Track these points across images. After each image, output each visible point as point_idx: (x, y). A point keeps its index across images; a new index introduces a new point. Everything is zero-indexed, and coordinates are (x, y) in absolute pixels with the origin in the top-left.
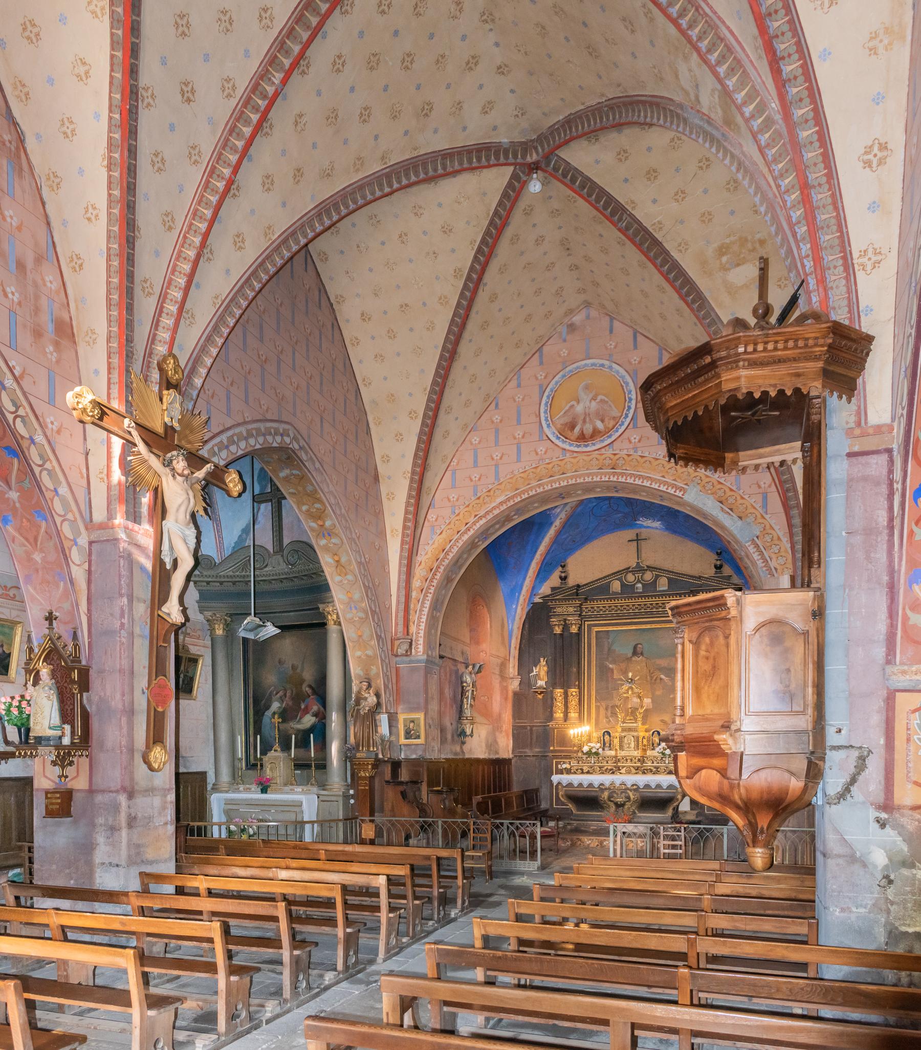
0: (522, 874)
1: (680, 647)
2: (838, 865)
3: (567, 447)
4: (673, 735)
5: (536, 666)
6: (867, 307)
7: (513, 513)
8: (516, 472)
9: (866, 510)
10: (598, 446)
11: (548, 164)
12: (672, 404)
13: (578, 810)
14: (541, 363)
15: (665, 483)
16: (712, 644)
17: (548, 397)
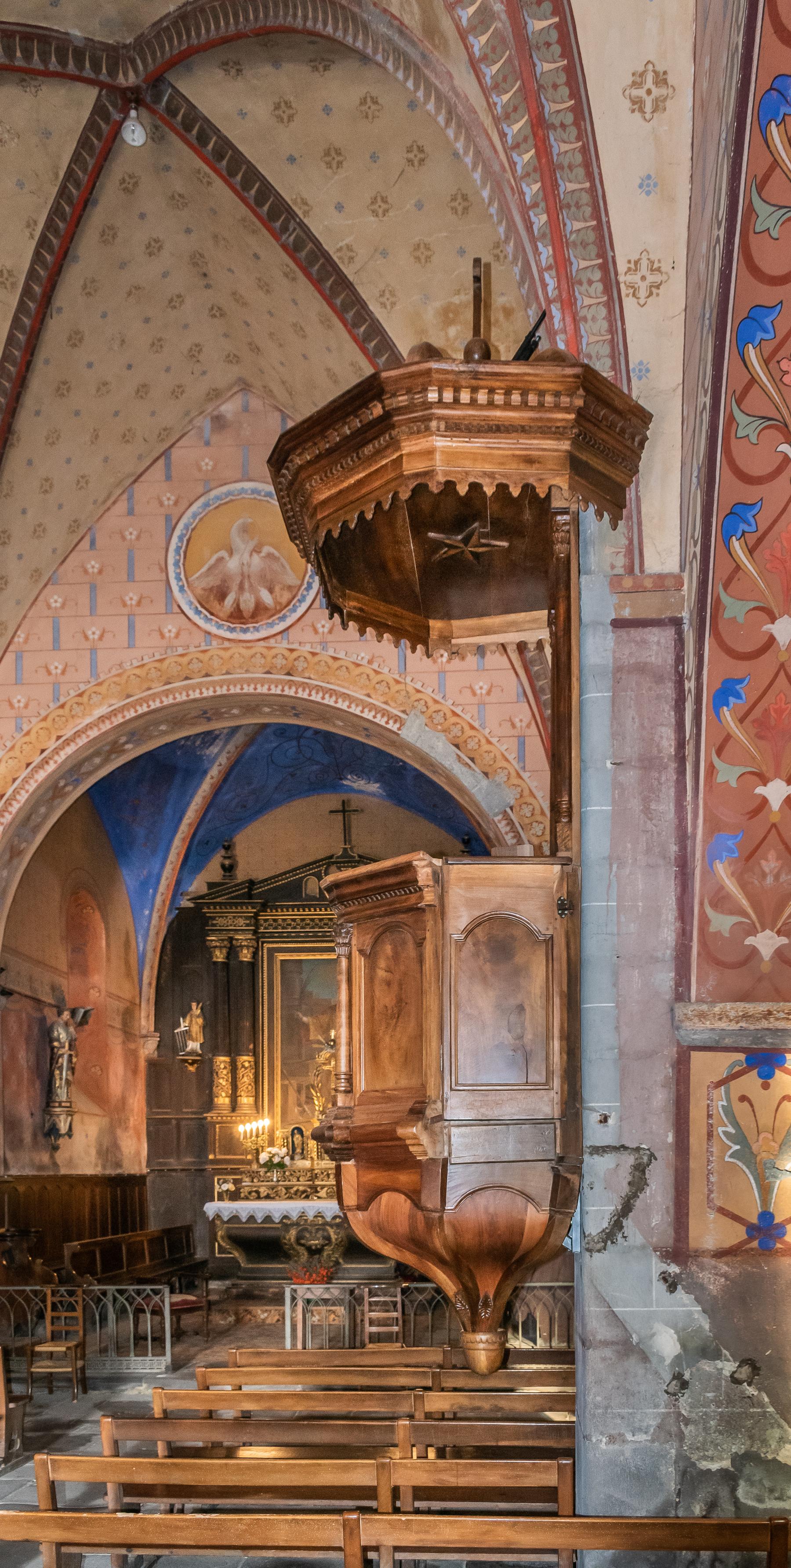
0: (139, 1379)
1: (344, 963)
2: (604, 1359)
3: (214, 630)
4: (331, 1128)
5: (184, 1017)
6: (641, 363)
7: (123, 739)
8: (127, 666)
9: (642, 726)
10: (263, 633)
11: (157, 99)
12: (322, 497)
13: (250, 1261)
14: (168, 478)
15: (372, 707)
16: (396, 957)
17: (181, 538)
